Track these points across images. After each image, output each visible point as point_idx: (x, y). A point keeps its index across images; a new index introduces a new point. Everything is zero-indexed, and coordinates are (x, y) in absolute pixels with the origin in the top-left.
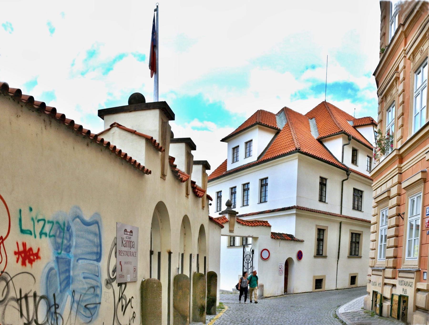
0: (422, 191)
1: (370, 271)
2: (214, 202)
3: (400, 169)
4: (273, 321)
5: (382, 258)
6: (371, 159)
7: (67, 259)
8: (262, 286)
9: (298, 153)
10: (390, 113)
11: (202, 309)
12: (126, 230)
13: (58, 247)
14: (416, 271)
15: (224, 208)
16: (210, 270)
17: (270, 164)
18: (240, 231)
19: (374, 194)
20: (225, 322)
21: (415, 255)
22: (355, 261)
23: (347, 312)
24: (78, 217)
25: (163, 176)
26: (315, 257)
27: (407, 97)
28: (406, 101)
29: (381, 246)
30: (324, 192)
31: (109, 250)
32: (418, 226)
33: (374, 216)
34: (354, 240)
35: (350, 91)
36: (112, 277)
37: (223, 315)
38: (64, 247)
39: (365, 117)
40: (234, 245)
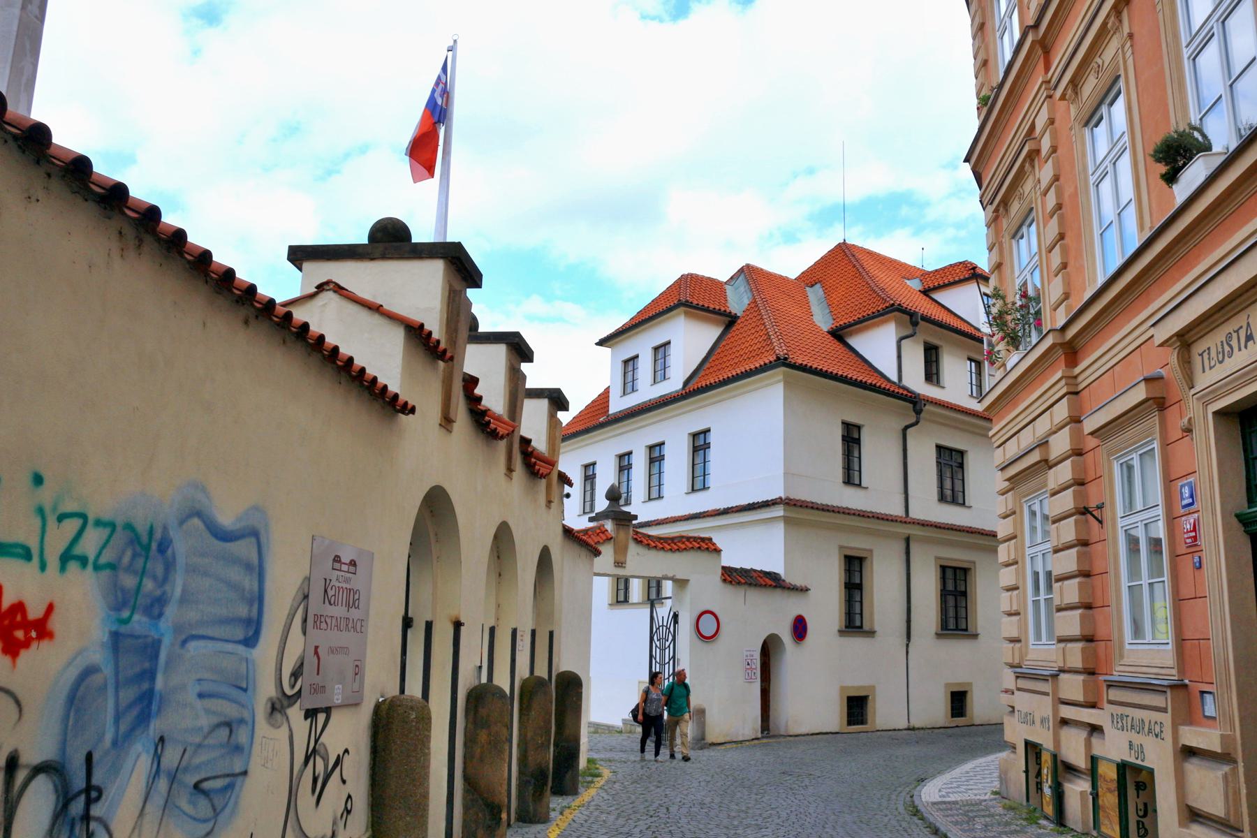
0: (1157, 435)
1: (1009, 679)
2: (576, 491)
3: (1070, 381)
4: (733, 814)
5: (1044, 640)
6: (979, 365)
7: (150, 640)
8: (701, 712)
9: (783, 369)
10: (1023, 242)
11: (541, 776)
12: (337, 559)
13: (121, 601)
14: (1171, 687)
15: (602, 504)
16: (564, 668)
17: (714, 396)
18: (642, 563)
19: (999, 457)
20: (603, 817)
21: (1158, 635)
22: (958, 649)
23: (947, 799)
24: (199, 514)
25: (447, 421)
26: (841, 633)
27: (1068, 191)
28: (1066, 200)
29: (1036, 603)
30: (856, 460)
31: (287, 612)
32: (1155, 544)
33: (1004, 518)
34: (950, 587)
35: (904, 211)
36: (289, 692)
37: (598, 794)
38: (142, 601)
39: (953, 262)
40: (626, 600)
